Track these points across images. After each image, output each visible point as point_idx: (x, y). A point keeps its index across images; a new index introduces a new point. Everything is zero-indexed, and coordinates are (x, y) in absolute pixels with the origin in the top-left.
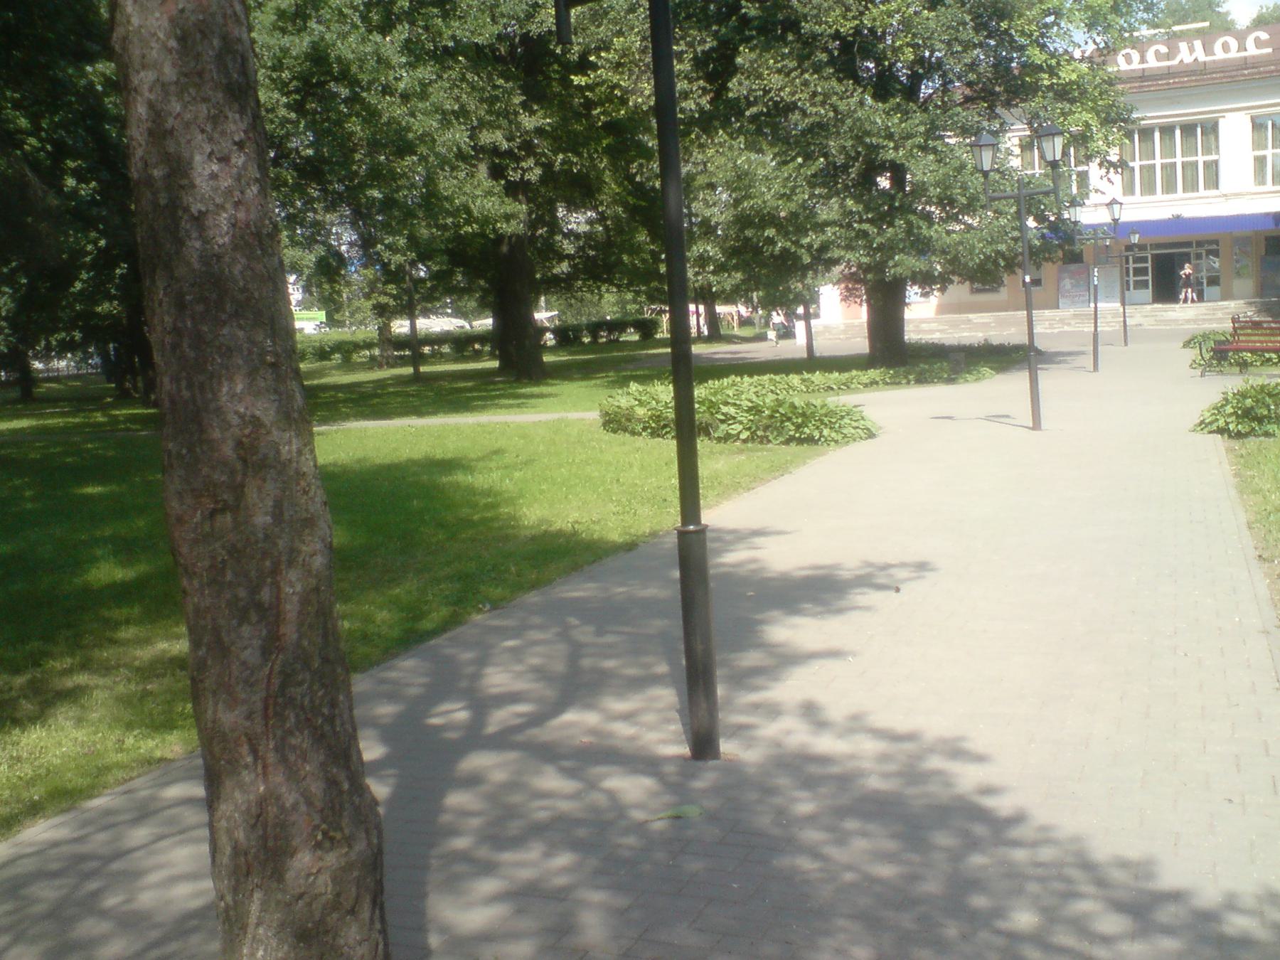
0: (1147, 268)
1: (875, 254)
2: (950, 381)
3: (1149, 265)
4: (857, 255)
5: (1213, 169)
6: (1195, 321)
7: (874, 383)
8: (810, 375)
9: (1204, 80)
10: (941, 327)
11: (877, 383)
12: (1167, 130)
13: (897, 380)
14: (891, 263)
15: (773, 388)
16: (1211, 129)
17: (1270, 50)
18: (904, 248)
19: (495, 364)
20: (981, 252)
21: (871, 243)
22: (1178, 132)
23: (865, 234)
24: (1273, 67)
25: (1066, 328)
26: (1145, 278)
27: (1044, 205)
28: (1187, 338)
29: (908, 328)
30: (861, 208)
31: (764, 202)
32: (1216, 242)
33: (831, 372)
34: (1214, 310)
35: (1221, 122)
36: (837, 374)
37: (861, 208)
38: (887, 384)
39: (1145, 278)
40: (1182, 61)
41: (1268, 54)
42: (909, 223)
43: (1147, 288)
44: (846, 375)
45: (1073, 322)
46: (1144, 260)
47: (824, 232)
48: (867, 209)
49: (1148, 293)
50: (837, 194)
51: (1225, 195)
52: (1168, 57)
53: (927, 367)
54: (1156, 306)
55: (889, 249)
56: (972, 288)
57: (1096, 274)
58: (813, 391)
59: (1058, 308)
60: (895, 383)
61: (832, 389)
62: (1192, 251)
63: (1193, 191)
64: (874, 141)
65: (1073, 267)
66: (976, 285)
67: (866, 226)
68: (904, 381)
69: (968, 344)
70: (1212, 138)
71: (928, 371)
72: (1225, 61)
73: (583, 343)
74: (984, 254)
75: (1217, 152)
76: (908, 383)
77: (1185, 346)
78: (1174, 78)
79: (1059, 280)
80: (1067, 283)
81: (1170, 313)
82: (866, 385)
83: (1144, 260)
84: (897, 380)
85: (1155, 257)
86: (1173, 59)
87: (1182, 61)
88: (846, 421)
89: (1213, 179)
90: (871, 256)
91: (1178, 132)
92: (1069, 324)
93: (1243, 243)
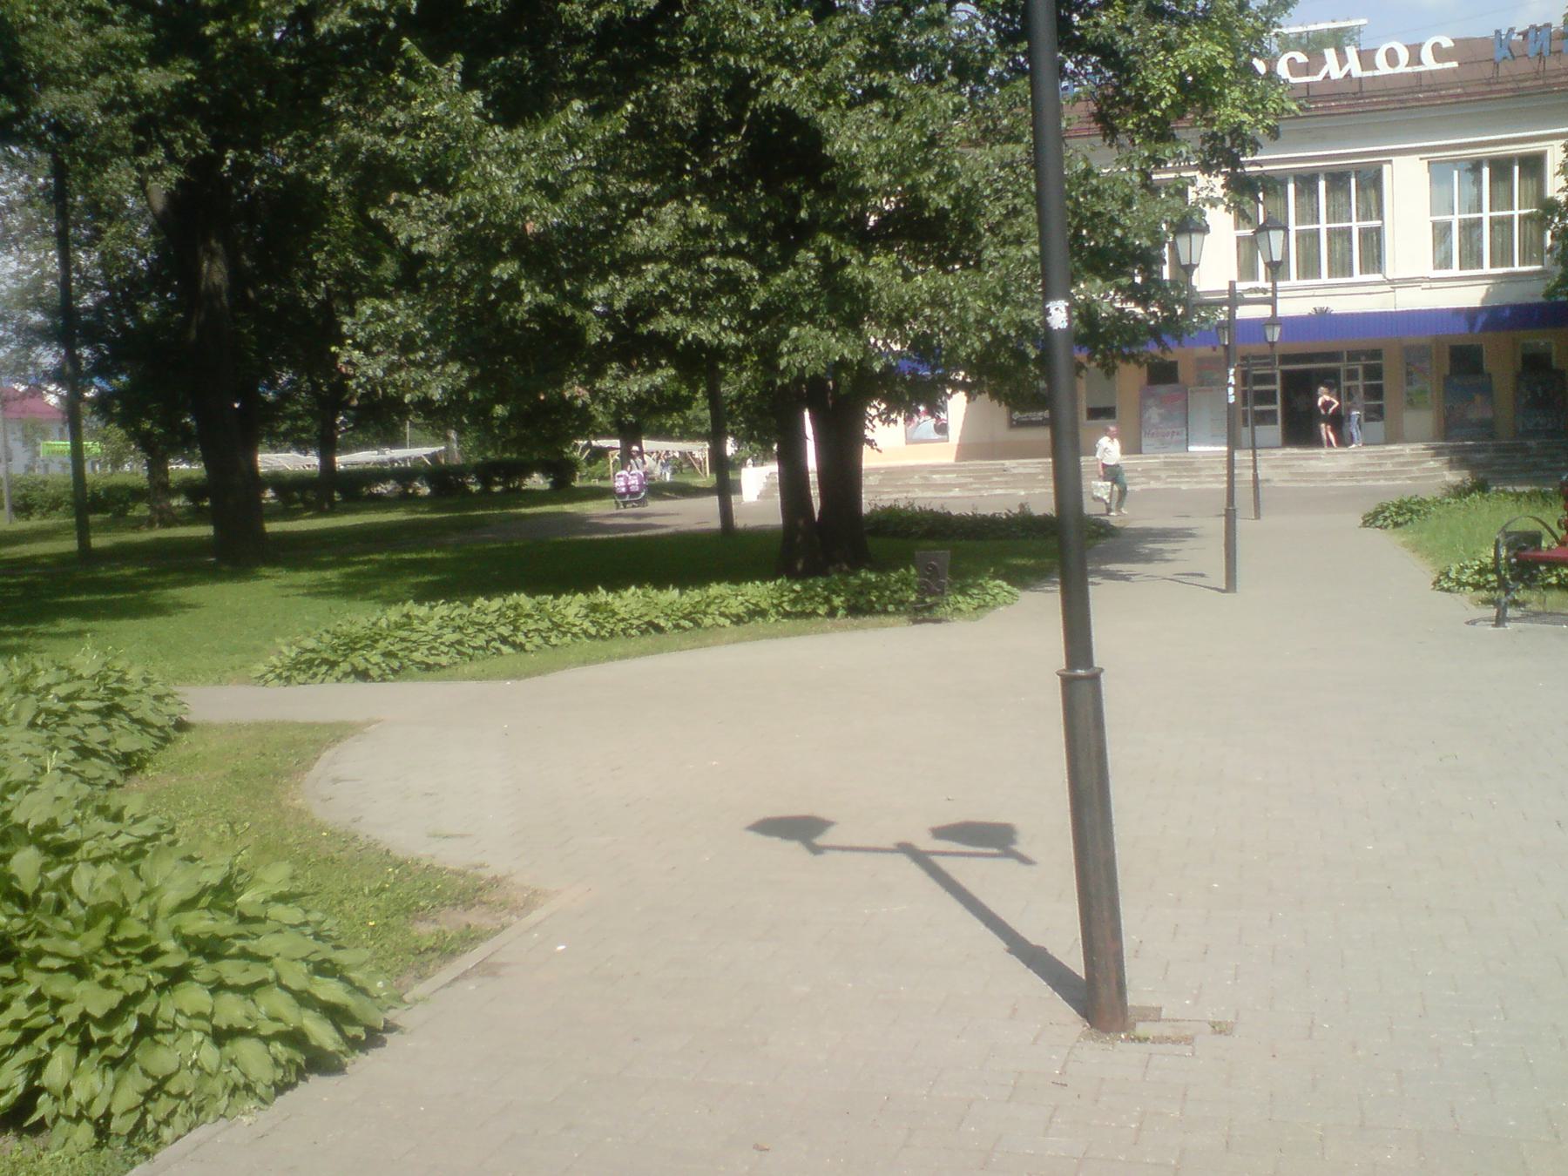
0: (1274, 392)
1: (757, 326)
2: (921, 612)
3: (1277, 387)
4: (716, 328)
5: (1373, 242)
6: (1352, 475)
7: (757, 613)
8: (610, 598)
9: (1358, 105)
10: (963, 481)
11: (763, 613)
12: (1307, 182)
13: (809, 607)
14: (785, 346)
15: (505, 631)
16: (1372, 180)
17: (1455, 64)
18: (814, 311)
19: (206, 531)
20: (981, 323)
21: (746, 300)
22: (1322, 185)
23: (730, 283)
24: (1459, 90)
25: (1153, 485)
26: (1272, 407)
27: (1122, 227)
28: (1371, 508)
29: (868, 482)
30: (721, 220)
31: (494, 199)
32: (1376, 354)
33: (661, 585)
34: (1380, 457)
35: (1386, 168)
36: (676, 592)
37: (721, 220)
38: (787, 615)
39: (1272, 407)
40: (1327, 77)
41: (1454, 70)
42: (824, 254)
43: (1275, 422)
44: (695, 595)
45: (1163, 475)
46: (1270, 379)
47: (639, 273)
48: (736, 224)
49: (1274, 431)
50: (678, 195)
51: (1391, 282)
52: (1307, 69)
53: (873, 577)
54: (1289, 450)
55: (780, 312)
56: (1011, 420)
57: (1232, 380)
58: (612, 633)
59: (1140, 451)
60: (799, 613)
61: (659, 629)
62: (1342, 366)
63: (1343, 276)
64: (745, 62)
65: (1162, 389)
66: (1017, 415)
67: (731, 263)
68: (822, 610)
69: (989, 512)
70: (1372, 194)
71: (876, 587)
72: (1390, 76)
73: (470, 492)
74: (994, 330)
75: (1380, 216)
76: (832, 613)
77: (1366, 524)
78: (1315, 102)
79: (1142, 408)
80: (1154, 414)
81: (1313, 462)
82: (738, 620)
83: (1270, 379)
84: (809, 607)
85: (1285, 374)
86: (1316, 74)
87: (1327, 77)
88: (193, 996)
89: (1374, 257)
90: (747, 332)
91: (1322, 185)
92: (1157, 478)
93: (1414, 358)
